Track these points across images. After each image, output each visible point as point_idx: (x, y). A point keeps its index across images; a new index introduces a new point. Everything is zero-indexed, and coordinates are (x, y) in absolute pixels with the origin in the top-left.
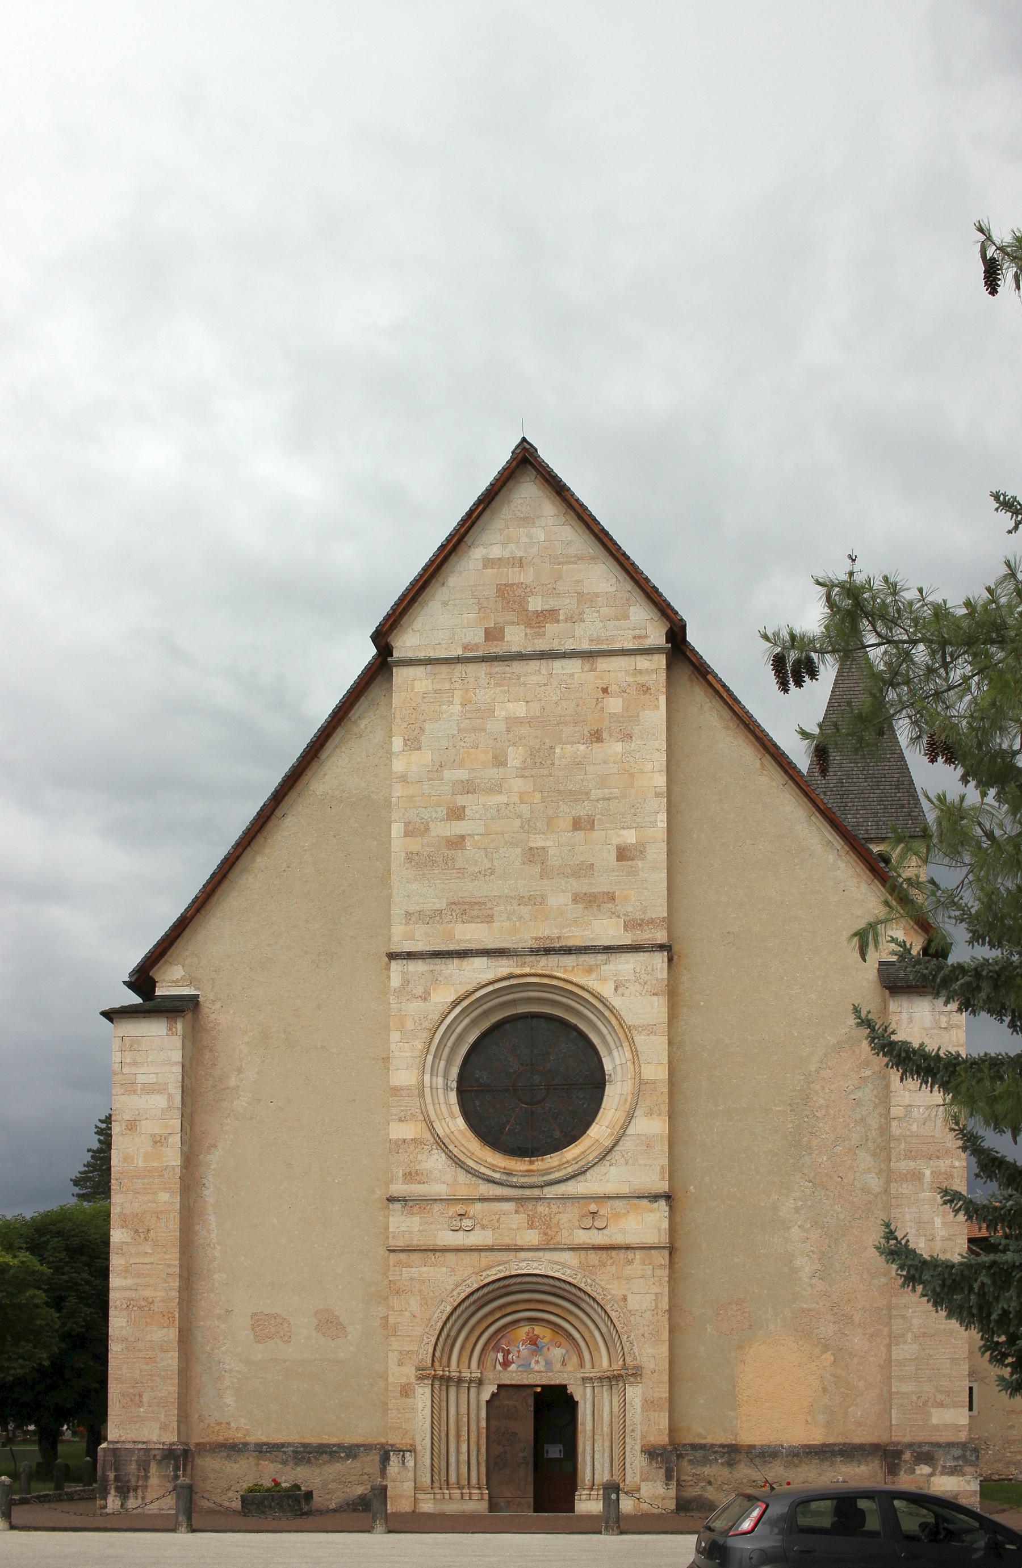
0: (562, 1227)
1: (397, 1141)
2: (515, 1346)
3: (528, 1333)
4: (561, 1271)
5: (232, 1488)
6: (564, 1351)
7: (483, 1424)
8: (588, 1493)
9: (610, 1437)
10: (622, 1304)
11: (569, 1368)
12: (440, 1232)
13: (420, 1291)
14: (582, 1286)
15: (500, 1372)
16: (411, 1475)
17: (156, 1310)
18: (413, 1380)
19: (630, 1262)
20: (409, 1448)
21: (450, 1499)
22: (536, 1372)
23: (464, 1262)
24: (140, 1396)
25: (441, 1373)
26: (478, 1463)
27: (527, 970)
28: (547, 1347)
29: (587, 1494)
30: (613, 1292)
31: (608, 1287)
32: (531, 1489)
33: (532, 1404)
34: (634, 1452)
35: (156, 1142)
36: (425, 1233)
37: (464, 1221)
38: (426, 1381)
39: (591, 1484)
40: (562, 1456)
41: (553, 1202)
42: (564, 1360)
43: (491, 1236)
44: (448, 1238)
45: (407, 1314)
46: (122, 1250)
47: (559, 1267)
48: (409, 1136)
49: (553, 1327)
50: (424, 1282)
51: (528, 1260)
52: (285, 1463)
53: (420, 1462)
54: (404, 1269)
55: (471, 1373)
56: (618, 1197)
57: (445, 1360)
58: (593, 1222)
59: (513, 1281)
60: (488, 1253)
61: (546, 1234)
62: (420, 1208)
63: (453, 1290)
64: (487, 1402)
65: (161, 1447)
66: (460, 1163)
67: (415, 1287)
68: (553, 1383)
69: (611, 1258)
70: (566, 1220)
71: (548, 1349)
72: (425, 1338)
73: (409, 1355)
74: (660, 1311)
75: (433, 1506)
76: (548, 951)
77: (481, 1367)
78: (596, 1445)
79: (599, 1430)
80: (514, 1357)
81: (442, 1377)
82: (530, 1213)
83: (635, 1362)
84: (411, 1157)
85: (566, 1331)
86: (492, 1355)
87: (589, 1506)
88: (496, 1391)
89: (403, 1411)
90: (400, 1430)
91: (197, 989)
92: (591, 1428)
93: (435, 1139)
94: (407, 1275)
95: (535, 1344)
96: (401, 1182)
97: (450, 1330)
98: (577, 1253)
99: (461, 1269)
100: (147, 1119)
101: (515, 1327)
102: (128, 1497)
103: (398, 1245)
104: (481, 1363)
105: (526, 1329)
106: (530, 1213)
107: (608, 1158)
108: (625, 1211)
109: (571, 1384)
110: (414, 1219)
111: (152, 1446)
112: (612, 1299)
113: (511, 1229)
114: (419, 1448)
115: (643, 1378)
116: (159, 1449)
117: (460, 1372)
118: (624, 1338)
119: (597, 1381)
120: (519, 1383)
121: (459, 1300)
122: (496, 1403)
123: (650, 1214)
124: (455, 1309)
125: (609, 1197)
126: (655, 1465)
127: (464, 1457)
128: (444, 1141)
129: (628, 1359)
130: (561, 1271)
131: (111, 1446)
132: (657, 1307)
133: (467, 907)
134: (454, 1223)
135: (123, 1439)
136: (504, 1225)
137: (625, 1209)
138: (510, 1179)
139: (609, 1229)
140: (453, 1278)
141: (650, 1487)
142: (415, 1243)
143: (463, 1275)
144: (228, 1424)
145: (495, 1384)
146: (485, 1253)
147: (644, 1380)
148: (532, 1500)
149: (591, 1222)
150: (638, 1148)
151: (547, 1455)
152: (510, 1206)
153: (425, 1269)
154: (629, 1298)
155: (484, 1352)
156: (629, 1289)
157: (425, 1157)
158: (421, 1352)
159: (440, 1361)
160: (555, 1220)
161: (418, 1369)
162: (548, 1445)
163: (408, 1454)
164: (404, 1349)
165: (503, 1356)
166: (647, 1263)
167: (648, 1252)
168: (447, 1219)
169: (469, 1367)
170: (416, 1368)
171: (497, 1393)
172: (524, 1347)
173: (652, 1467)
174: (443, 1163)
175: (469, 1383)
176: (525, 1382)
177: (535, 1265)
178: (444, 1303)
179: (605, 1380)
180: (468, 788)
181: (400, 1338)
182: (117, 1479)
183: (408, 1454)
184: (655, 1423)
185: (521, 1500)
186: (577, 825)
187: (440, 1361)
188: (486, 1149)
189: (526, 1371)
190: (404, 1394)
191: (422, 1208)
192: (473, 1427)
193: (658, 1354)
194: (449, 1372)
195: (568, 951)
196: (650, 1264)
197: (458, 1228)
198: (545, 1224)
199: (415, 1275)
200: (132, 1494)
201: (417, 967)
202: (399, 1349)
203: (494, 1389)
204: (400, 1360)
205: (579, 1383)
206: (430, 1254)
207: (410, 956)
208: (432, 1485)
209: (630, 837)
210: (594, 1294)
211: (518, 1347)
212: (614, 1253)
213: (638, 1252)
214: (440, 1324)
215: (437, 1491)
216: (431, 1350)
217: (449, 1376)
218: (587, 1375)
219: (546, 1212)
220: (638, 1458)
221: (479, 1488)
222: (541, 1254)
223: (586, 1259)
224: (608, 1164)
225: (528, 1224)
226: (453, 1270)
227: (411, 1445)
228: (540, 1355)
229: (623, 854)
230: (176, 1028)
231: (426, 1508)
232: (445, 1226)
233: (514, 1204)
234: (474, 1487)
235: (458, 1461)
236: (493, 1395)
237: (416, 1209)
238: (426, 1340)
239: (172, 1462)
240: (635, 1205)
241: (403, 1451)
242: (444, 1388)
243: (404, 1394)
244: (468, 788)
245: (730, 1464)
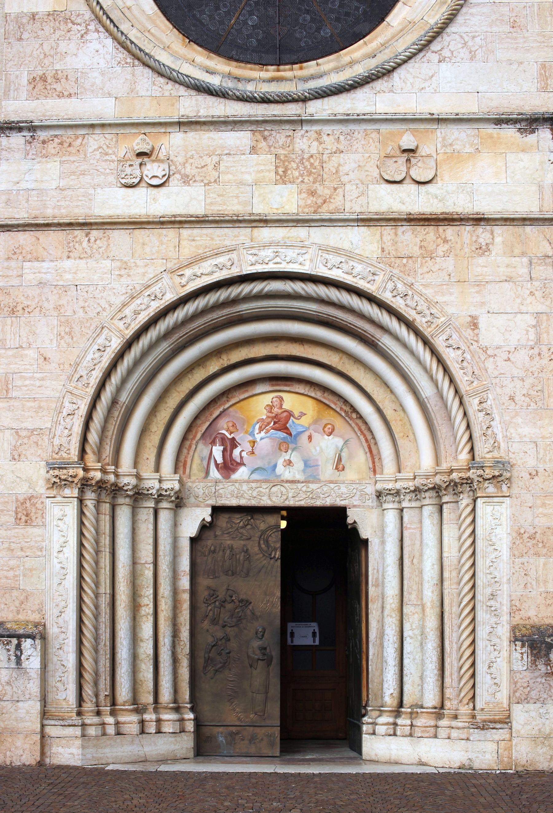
0: (345, 179)
1: (19, 16)
2: (246, 432)
3: (270, 408)
4: (345, 267)
6: (339, 442)
7: (185, 583)
8: (391, 720)
9: (438, 610)
10: (468, 333)
11: (350, 474)
12: (99, 190)
13: (57, 308)
14: (387, 297)
15: (217, 482)
16: (34, 687)
18: (41, 488)
20: (30, 629)
21: (118, 733)
22: (287, 481)
23: (147, 249)
25: (98, 475)
26: (175, 660)
28: (307, 434)
29: (387, 724)
30: (450, 310)
31: (439, 298)
32: (275, 709)
33: (279, 545)
34: (495, 640)
36: (68, 193)
37: (149, 166)
38: (67, 492)
39: (395, 703)
40: (317, 643)
41: (327, 129)
42: (340, 459)
43: (202, 197)
45: (31, 353)
47: (339, 259)
49: (318, 395)
50: (65, 289)
51: (277, 244)
53: (55, 659)
54: (27, 265)
55: (160, 481)
56: (458, 120)
57: (108, 450)
58: (408, 169)
59: (246, 289)
60: (196, 232)
61: (313, 193)
62: (61, 144)
63: (124, 305)
64: (193, 540)
66: (142, 55)
67: (47, 299)
68: (319, 503)
69: (446, 241)
70: (354, 165)
71: (310, 438)
72: (67, 404)
73: (34, 438)
74: (544, 349)
75: (80, 751)
77: (181, 470)
78: (406, 626)
79: (413, 597)
80: (244, 454)
81: (101, 485)
82: (281, 151)
83: (496, 454)
84: (46, 47)
85: (346, 401)
86: (202, 450)
87: (393, 747)
88: (209, 519)
89: (20, 553)
90: (15, 593)
92: (397, 591)
93: (93, 12)
94: (31, 276)
95: (284, 428)
96: (24, 95)
97: (119, 389)
98: (376, 231)
99: (139, 263)
101: (246, 395)
103: (17, 216)
104: (181, 464)
105: (267, 399)
106: (281, 151)
107: (435, 46)
108: (472, 150)
109: (355, 506)
110: (49, 166)
112: (448, 324)
113: (242, 183)
114: (53, 630)
115: (514, 486)
117: (138, 477)
118: (473, 404)
119: (408, 497)
120: (253, 503)
121: (135, 326)
122: (209, 542)
123: (521, 155)
124: (128, 345)
125: (440, 121)
126: (543, 668)
127: (147, 648)
128: (112, 17)
129: (481, 449)
130: (345, 267)
132: (538, 341)
134: (128, 170)
136: (230, 177)
137: (472, 145)
138: (240, 86)
139: (440, 183)
140: (125, 281)
141: (533, 714)
142: (49, 212)
143: (144, 274)
145: (207, 506)
146: (189, 231)
147: (515, 491)
148: (277, 731)
149: (404, 169)
150: (495, 29)
151: (292, 642)
153: (68, 264)
154: (482, 322)
155: (187, 443)
156: (483, 304)
157: (72, 46)
158: (58, 433)
159: (99, 453)
160: (330, 166)
161: (51, 466)
162: (294, 624)
163: (27, 644)
164: (23, 425)
165: (224, 451)
166: (517, 251)
167: (519, 230)
168: (113, 165)
169: (157, 469)
170: (48, 464)
171: (211, 523)
172: (263, 434)
173: (537, 673)
174: (108, 57)
175: (158, 501)
176: (266, 502)
177: (291, 254)
178: (105, 331)
179: (427, 494)
181: (16, 403)
183: (27, 644)
184: (537, 580)
185: (257, 730)
187: (99, 453)
188: (194, 50)
189: (266, 481)
190: (24, 518)
191: (66, 145)
192: (165, 589)
193: (543, 437)
194: (117, 475)
196: (523, 254)
197: (136, 181)
198: (310, 174)
199: (49, 277)
202: (15, 426)
203: (206, 514)
204: (15, 448)
205: (369, 503)
206: (79, 233)
208: (80, 706)
210: (410, 314)
211: (252, 434)
212: (450, 231)
213: (498, 230)
214: (97, 375)
215: (91, 719)
216: (78, 429)
217: (115, 485)
218: (390, 486)
219: (313, 151)
220: (505, 654)
221: (177, 710)
222: (301, 232)
223: (395, 243)
224: (435, 58)
225: (277, 173)
226: (125, 266)
227: (36, 625)
228: (293, 450)
231: (66, 755)
232: (111, 179)
233: (248, 134)
234: (166, 708)
235: (134, 658)
236: (204, 527)
237: (52, 147)
238: (68, 407)
240: (491, 137)
241: (19, 637)
242: (106, 508)
243: (24, 518)
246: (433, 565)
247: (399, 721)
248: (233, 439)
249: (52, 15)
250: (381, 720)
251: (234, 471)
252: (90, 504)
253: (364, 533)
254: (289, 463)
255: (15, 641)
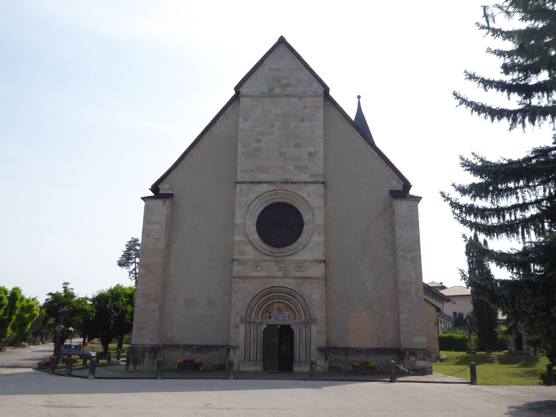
3: (277, 307)
5: (174, 362)
7: (262, 338)
14: (296, 291)
15: (268, 320)
17: (152, 297)
19: (312, 283)
20: (237, 347)
24: (144, 327)
27: (279, 188)
35: (156, 240)
38: (243, 323)
44: (252, 273)
46: (142, 276)
48: (240, 240)
52: (193, 352)
64: (263, 330)
65: (150, 346)
71: (284, 312)
76: (286, 183)
81: (249, 322)
86: (265, 314)
91: (173, 192)
95: (280, 311)
100: (153, 232)
102: (137, 365)
111: (147, 346)
116: (149, 347)
118: (310, 309)
131: (132, 346)
133: (261, 169)
135: (137, 343)
144: (174, 338)
152: (273, 263)
180: (262, 133)
182: (133, 358)
183: (236, 349)
186: (296, 145)
195: (293, 183)
200: (138, 364)
201: (244, 186)
207: (243, 183)
209: (312, 150)
210: (300, 294)
224: (305, 250)
229: (310, 155)
230: (166, 203)
239: (154, 352)
241: (235, 348)
244: (262, 133)
245: (346, 354)
246: (264, 65)
247: (299, 364)
248: (271, 313)
249: (242, 241)
250: (296, 364)
251: (271, 318)
252: (247, 325)
253: (294, 330)
254: (281, 317)
255: (234, 349)
